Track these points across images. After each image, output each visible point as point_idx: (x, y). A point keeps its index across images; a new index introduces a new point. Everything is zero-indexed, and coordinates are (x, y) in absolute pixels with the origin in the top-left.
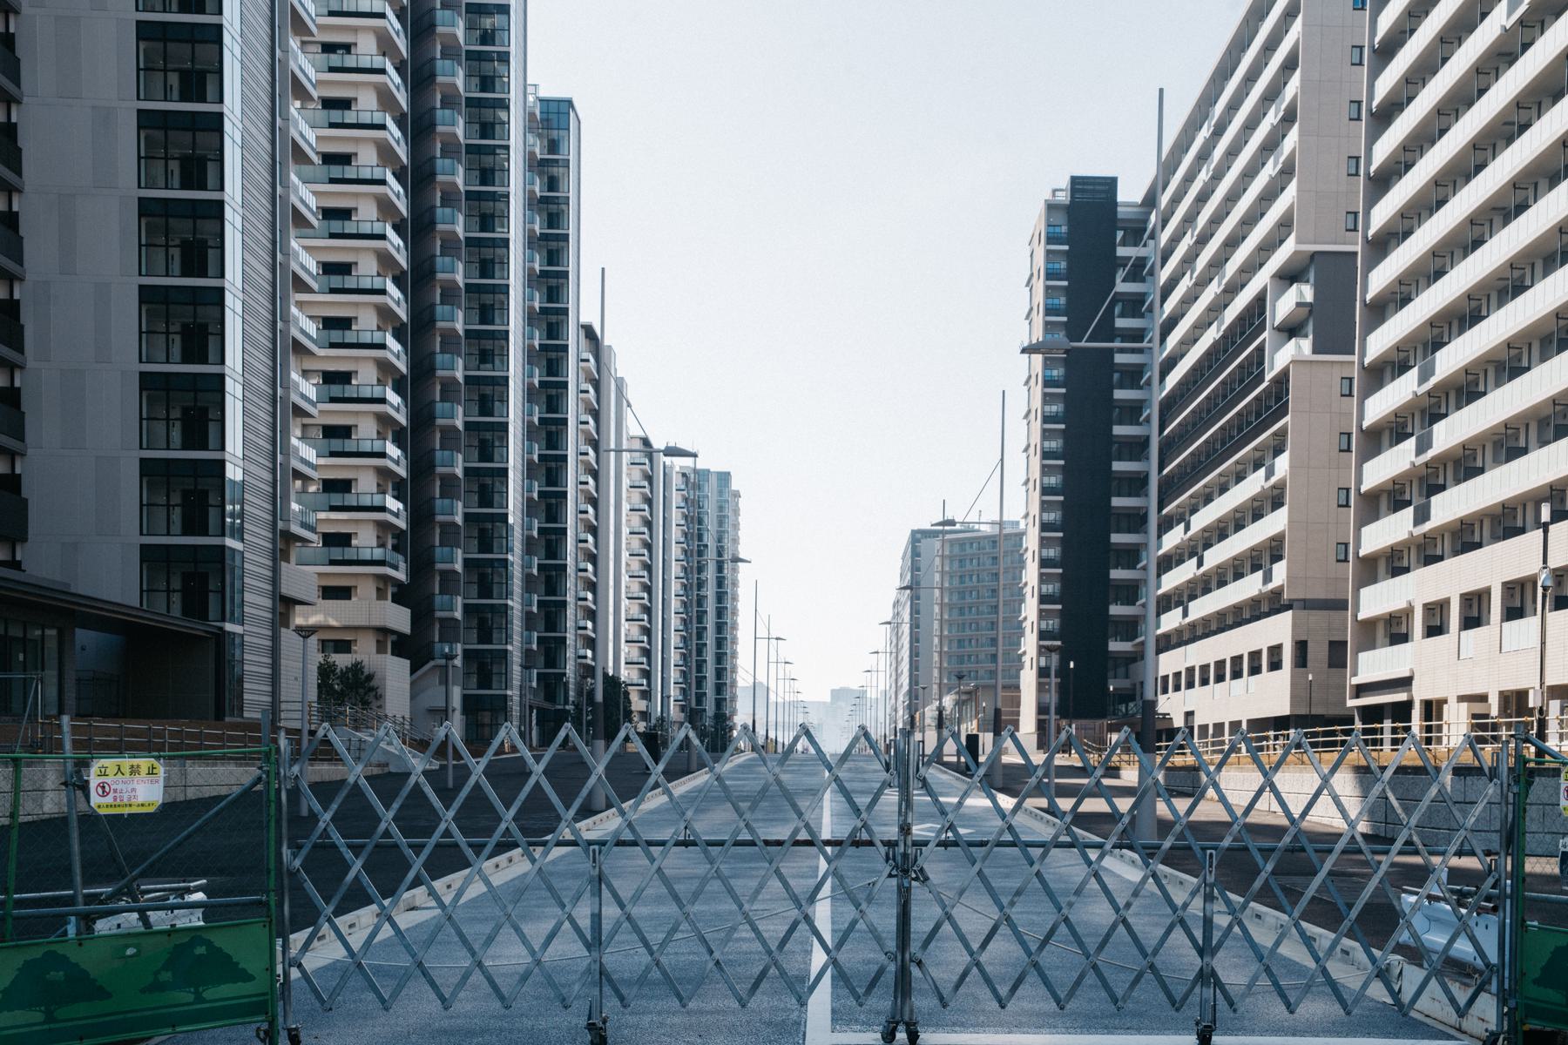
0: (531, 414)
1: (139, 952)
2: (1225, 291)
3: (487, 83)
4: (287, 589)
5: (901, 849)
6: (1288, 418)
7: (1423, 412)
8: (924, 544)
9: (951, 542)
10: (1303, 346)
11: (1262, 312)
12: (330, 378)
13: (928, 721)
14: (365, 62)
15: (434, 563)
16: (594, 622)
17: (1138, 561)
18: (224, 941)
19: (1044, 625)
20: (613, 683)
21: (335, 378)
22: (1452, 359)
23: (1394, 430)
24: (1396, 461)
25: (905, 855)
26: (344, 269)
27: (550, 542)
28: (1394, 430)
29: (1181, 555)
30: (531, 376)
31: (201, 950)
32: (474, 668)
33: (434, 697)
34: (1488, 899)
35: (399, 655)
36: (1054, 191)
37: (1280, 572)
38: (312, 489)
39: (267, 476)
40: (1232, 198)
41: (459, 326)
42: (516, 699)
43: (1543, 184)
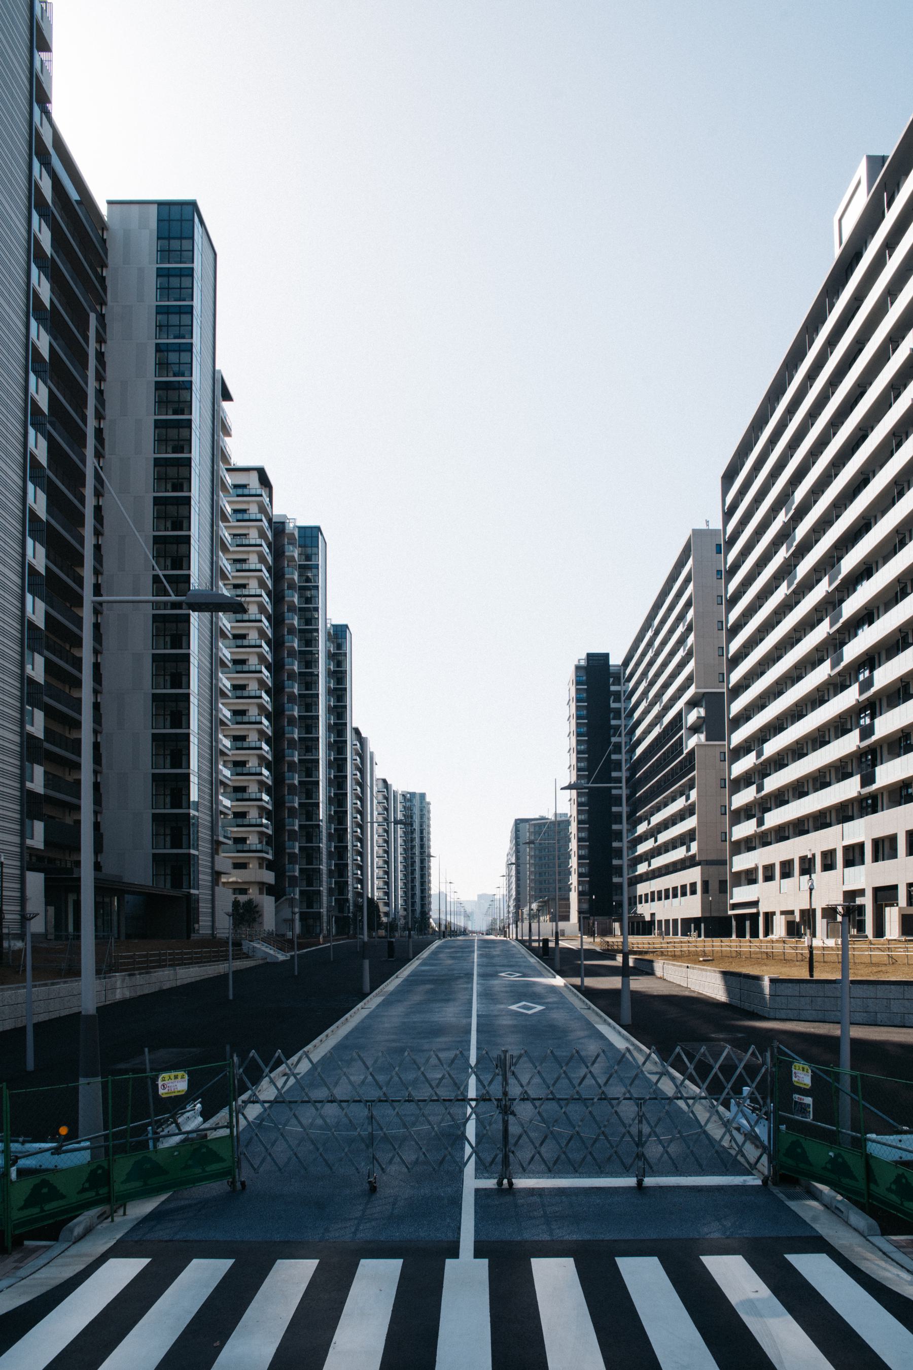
1: (179, 1154)
2: (663, 709)
6: (695, 772)
9: (535, 825)
11: (681, 720)
13: (525, 916)
15: (285, 849)
20: (371, 901)
21: (238, 739)
22: (772, 747)
26: (243, 687)
27: (339, 835)
29: (647, 836)
30: (330, 737)
33: (286, 913)
35: (270, 895)
36: (579, 660)
37: (694, 846)
40: (665, 665)
42: (325, 913)
43: (809, 667)
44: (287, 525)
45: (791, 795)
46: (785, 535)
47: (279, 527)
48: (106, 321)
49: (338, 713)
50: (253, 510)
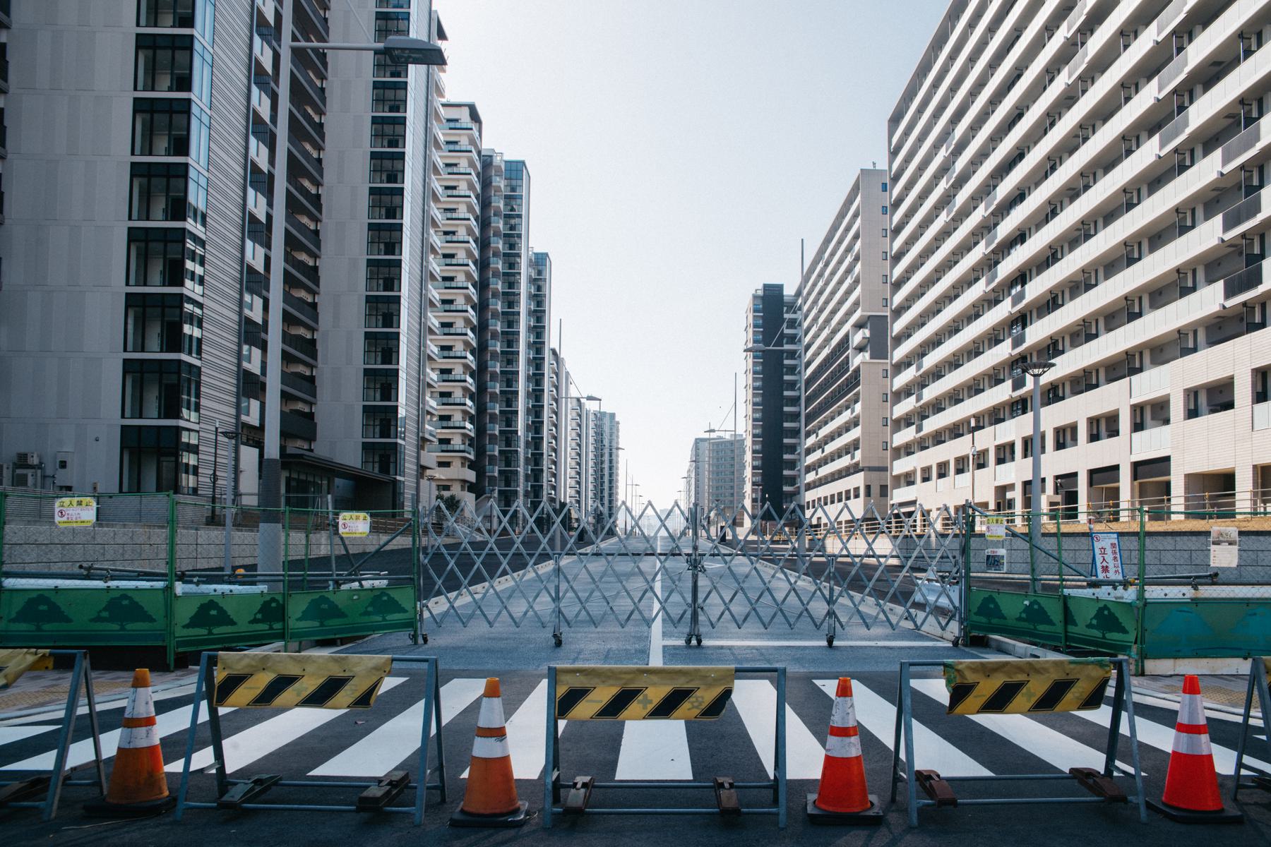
0: (528, 387)
2: (831, 332)
3: (512, 246)
4: (423, 462)
5: (693, 557)
6: (860, 387)
7: (918, 384)
8: (701, 445)
10: (866, 356)
11: (848, 341)
12: (443, 371)
14: (461, 239)
16: (556, 453)
17: (796, 451)
18: (396, 594)
19: (754, 480)
22: (930, 360)
23: (906, 392)
24: (906, 406)
25: (695, 560)
26: (450, 325)
27: (536, 442)
28: (906, 392)
31: (385, 598)
32: (503, 498)
34: (954, 578)
37: (858, 454)
38: (435, 419)
39: (416, 413)
40: (833, 293)
41: (498, 349)
44: (494, 158)
45: (947, 403)
46: (944, 169)
47: (487, 162)
48: (326, 95)
49: (537, 333)
50: (464, 143)
